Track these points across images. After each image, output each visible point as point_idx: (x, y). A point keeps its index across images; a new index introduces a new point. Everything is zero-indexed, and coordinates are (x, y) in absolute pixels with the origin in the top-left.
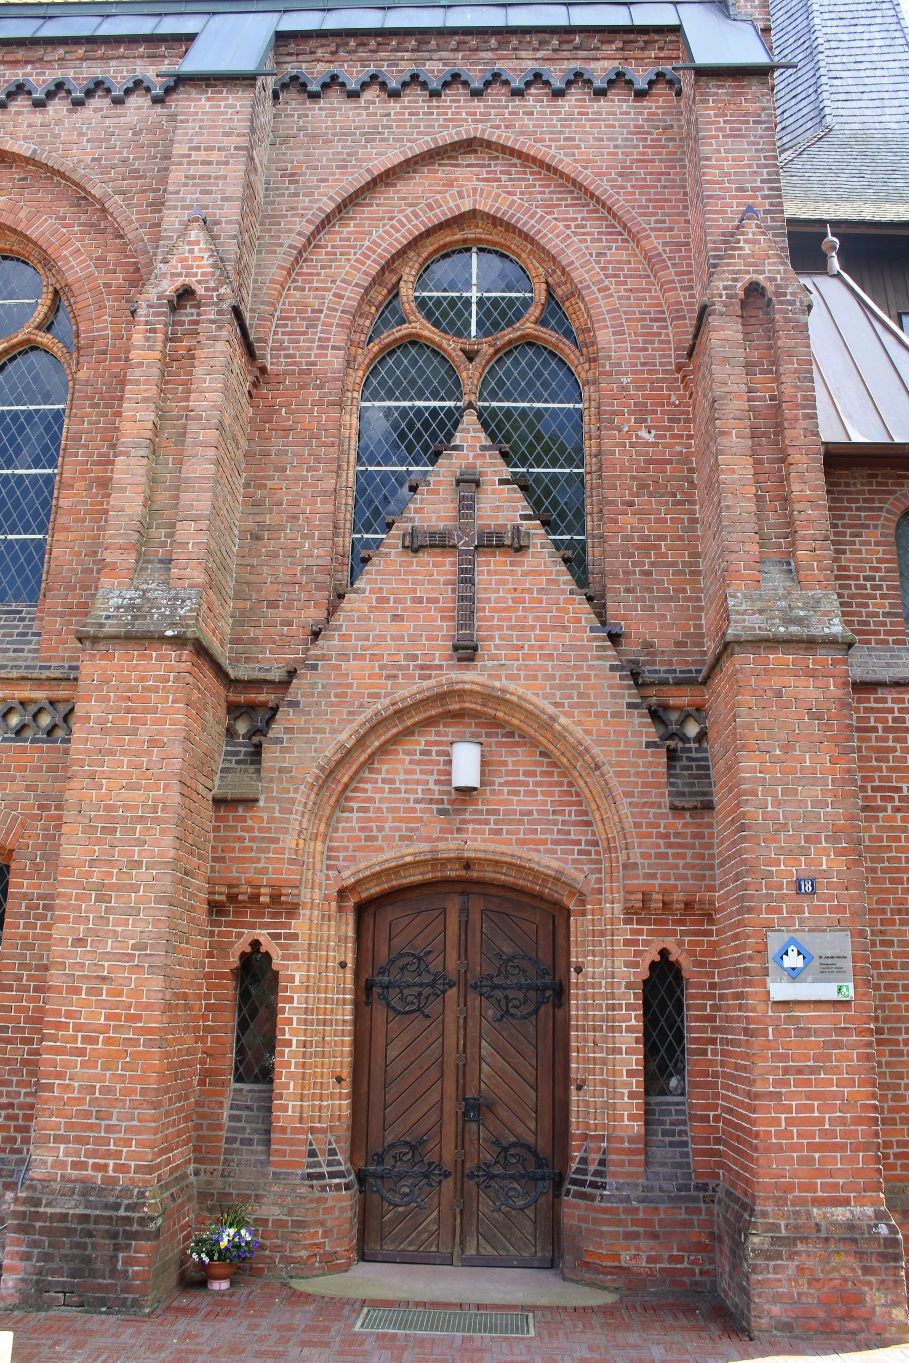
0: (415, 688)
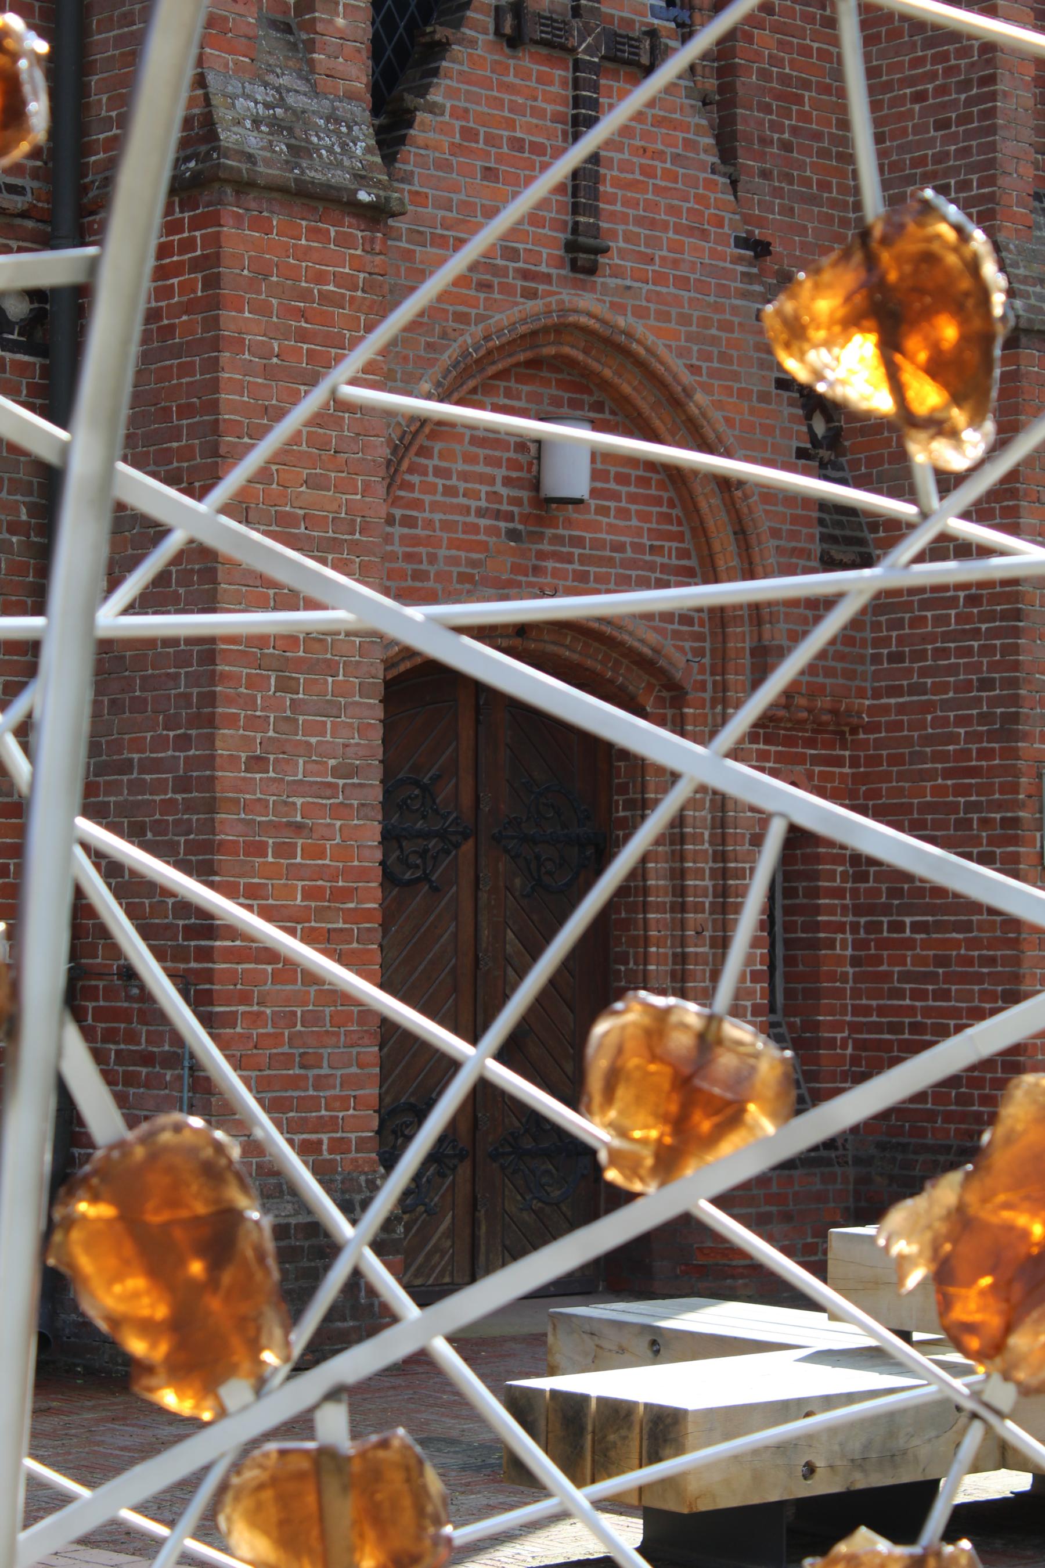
0: (515, 313)
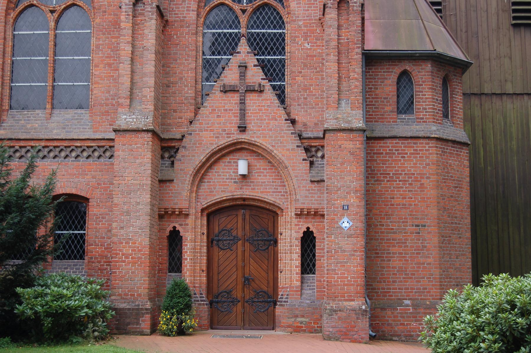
0: (225, 141)
